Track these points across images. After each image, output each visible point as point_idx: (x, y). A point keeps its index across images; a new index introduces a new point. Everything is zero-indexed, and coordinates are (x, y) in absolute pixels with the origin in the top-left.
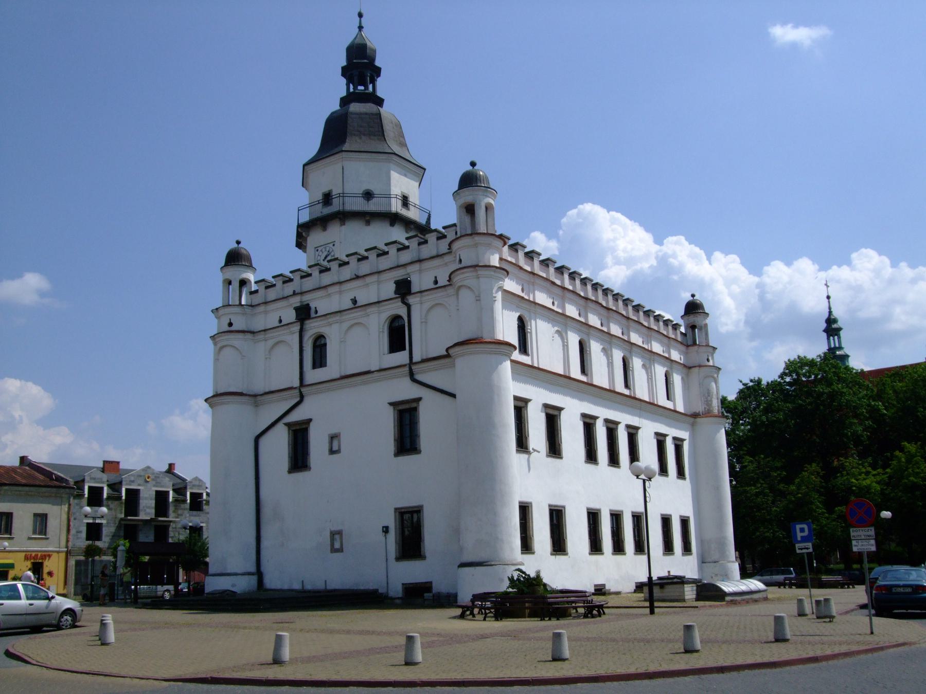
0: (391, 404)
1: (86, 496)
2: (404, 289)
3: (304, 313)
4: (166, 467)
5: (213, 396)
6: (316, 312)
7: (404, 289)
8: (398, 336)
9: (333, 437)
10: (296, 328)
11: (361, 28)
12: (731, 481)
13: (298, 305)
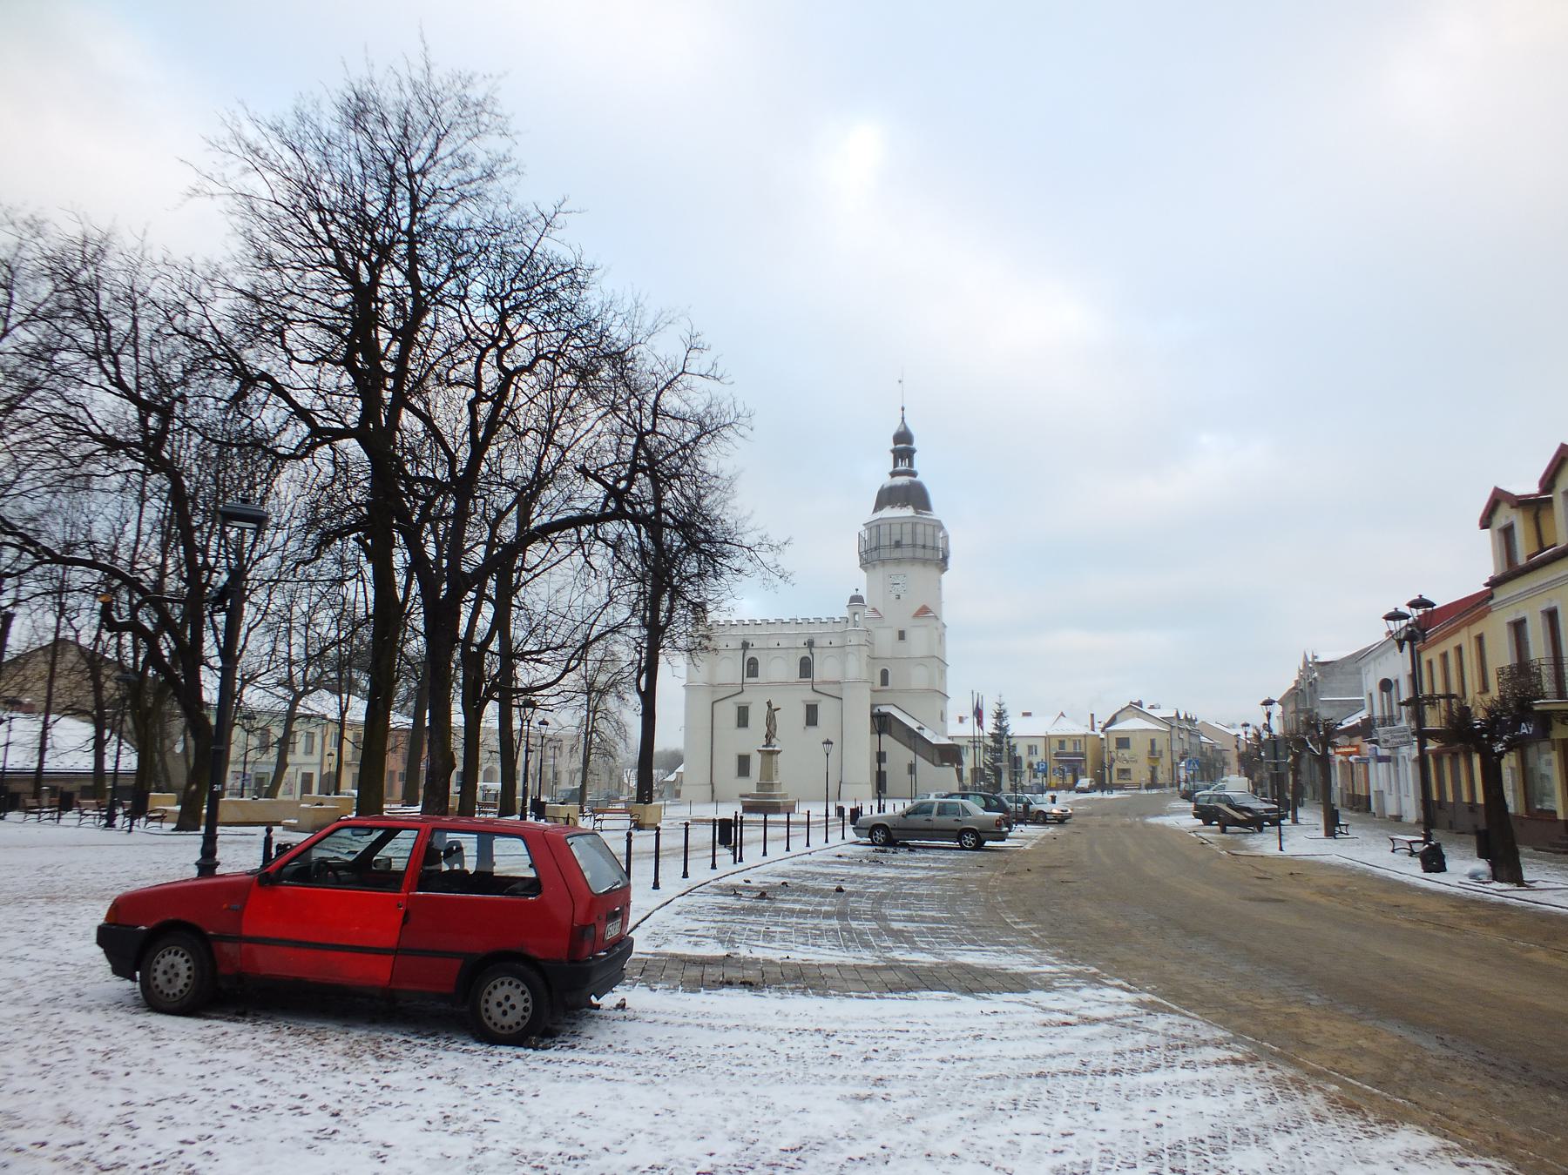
3: (745, 646)
7: (810, 644)
8: (806, 668)
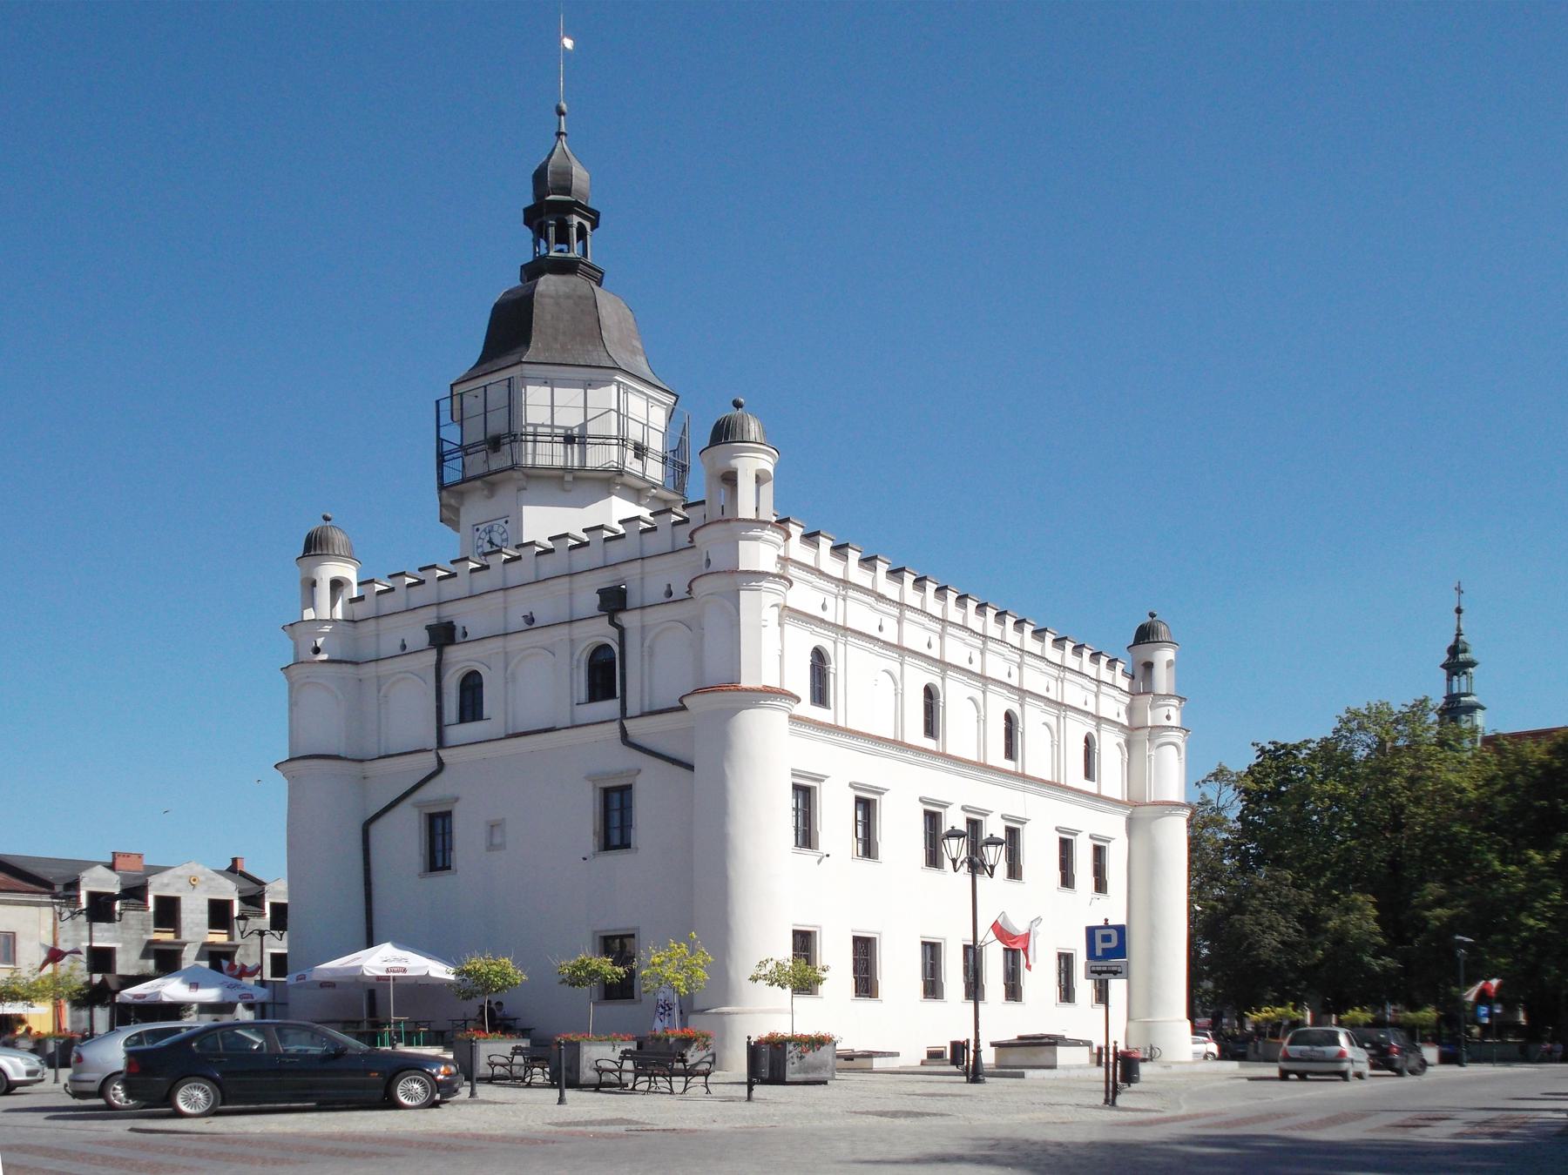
0: (589, 778)
1: (152, 909)
2: (614, 601)
3: (443, 635)
4: (230, 864)
5: (291, 760)
6: (465, 634)
8: (604, 675)
9: (493, 827)
10: (432, 656)
12: (1190, 903)
13: (434, 622)
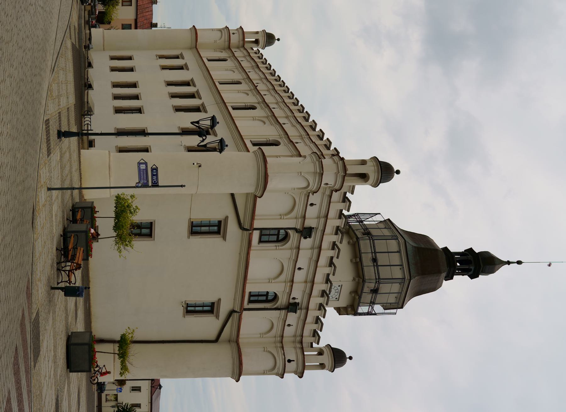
3: (306, 232)
7: (292, 307)
11: (509, 263)
